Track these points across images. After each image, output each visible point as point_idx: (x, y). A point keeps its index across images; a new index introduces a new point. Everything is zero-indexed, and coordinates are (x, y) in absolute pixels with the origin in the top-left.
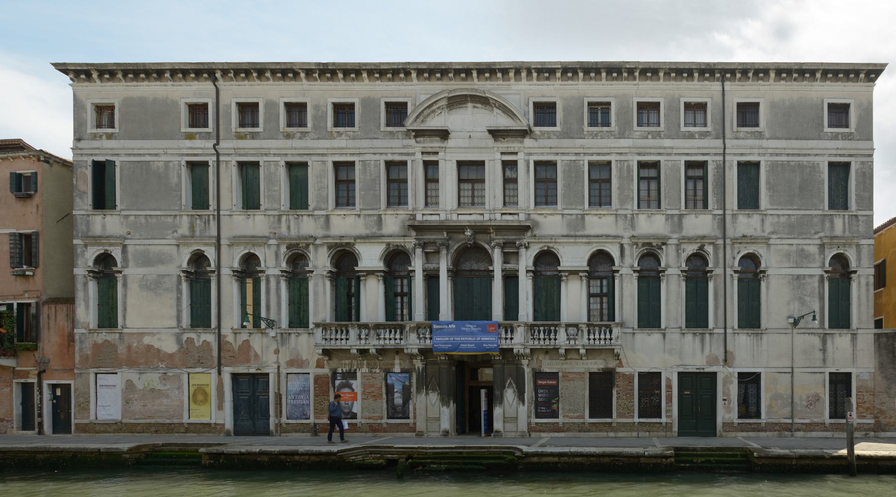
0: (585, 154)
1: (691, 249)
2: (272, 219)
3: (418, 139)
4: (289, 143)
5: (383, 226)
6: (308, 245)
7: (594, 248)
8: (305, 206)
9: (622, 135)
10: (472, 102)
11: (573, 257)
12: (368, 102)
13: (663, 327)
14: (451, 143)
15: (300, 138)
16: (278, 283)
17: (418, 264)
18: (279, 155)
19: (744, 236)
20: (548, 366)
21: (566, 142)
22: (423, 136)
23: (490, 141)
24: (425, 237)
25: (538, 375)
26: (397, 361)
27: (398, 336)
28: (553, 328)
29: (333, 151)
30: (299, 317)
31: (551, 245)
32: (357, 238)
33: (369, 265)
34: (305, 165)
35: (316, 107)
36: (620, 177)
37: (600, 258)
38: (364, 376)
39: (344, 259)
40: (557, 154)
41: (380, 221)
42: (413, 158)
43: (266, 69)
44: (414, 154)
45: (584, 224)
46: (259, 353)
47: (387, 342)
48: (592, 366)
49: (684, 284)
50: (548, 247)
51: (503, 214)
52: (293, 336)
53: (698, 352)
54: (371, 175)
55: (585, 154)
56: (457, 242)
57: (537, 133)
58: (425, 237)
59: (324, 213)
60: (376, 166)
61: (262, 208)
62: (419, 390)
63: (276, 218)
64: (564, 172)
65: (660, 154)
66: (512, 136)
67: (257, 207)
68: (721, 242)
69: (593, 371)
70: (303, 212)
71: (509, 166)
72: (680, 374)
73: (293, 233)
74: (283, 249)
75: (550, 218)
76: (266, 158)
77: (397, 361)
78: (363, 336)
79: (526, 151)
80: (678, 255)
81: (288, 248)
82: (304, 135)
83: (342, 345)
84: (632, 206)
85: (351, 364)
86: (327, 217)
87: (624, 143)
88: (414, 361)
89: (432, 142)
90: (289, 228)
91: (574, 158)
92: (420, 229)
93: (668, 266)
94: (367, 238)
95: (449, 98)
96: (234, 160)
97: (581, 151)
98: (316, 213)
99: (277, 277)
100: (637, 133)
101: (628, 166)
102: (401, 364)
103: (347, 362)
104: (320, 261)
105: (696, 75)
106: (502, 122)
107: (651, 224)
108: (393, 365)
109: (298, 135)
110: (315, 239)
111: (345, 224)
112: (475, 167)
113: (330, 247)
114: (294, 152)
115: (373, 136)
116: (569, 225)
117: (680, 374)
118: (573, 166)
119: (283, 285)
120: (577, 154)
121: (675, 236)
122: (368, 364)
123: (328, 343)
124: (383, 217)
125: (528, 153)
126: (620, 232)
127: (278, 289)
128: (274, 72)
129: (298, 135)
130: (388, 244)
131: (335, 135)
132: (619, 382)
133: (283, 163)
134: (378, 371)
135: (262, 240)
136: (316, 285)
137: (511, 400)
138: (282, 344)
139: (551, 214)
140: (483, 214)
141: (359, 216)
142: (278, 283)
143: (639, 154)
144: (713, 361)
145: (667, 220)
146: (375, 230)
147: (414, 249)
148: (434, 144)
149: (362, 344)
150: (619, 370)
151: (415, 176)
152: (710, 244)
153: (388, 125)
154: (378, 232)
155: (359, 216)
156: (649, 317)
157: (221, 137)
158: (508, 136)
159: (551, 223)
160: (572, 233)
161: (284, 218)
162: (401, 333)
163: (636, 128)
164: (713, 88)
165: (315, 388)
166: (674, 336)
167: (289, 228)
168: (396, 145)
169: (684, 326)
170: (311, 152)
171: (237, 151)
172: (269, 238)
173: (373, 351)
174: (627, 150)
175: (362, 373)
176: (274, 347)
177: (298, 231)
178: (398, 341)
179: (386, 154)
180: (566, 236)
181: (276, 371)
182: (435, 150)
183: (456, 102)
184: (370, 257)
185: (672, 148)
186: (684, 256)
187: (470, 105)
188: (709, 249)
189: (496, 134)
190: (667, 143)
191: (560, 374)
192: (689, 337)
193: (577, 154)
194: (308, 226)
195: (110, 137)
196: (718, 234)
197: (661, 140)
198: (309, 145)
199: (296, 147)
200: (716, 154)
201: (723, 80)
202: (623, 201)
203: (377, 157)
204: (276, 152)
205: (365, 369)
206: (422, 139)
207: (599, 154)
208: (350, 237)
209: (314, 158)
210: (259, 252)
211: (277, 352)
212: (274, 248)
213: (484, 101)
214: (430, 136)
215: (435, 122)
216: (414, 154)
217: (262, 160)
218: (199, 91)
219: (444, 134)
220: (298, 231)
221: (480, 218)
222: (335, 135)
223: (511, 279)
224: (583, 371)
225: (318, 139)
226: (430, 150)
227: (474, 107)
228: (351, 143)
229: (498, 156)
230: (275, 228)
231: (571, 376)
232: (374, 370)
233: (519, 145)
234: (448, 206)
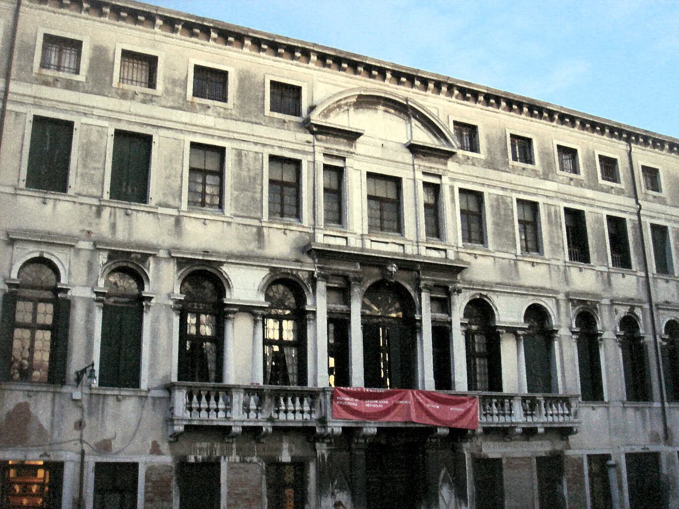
0: (512, 190)
1: (623, 311)
2: (86, 209)
3: (319, 136)
4: (126, 105)
5: (266, 243)
6: (146, 257)
7: (530, 301)
8: (143, 197)
9: (546, 177)
10: (384, 105)
11: (509, 312)
12: (245, 78)
13: (606, 400)
14: (360, 146)
15: (144, 102)
16: (89, 311)
17: (320, 304)
18: (109, 119)
19: (667, 302)
20: (492, 450)
21: (492, 174)
22: (327, 134)
23: (408, 157)
24: (335, 267)
25: (481, 462)
26: (285, 446)
27: (306, 408)
28: (507, 400)
29: (195, 129)
30: (121, 366)
31: (484, 293)
32: (230, 255)
33: (242, 298)
34: (147, 140)
35: (541, 144)
36: (550, 222)
37: (536, 313)
38: (231, 466)
39: (204, 281)
40: (483, 184)
41: (260, 235)
42: (310, 158)
43: (650, 137)
44: (313, 156)
45: (517, 271)
46: (46, 425)
47: (291, 416)
48: (540, 449)
49: (620, 351)
50: (481, 294)
51: (427, 248)
52: (111, 402)
53: (641, 430)
54: (249, 170)
55: (512, 190)
56: (370, 278)
57: (460, 156)
58: (335, 267)
59: (174, 212)
60: (256, 159)
61: (70, 192)
62: (321, 489)
63: (94, 209)
64: (492, 206)
65: (584, 204)
66: (435, 156)
67: (60, 185)
68: (647, 306)
69: (540, 454)
70: (142, 207)
71: (434, 189)
72: (628, 456)
73: (121, 235)
74: (103, 258)
75: (480, 259)
76: (85, 120)
77: (285, 446)
78: (253, 406)
79: (450, 175)
80: (612, 317)
81: (110, 258)
82: (148, 100)
83: (218, 419)
84: (564, 257)
85: (212, 449)
86: (178, 221)
87: (550, 185)
88: (317, 445)
89: (338, 143)
90: (113, 226)
91: (501, 193)
92: (324, 255)
93: (604, 330)
94: (244, 259)
95: (360, 96)
96: (32, 112)
97: (508, 186)
98: (161, 210)
99: (89, 301)
100: (561, 178)
101: (556, 212)
102: (290, 450)
103: (205, 445)
104: (164, 283)
105: (667, 147)
106: (423, 137)
107: (584, 280)
108: (280, 450)
109: (141, 97)
110: (157, 249)
111: (205, 234)
112: (383, 182)
113: (181, 263)
114: (133, 119)
115: (254, 120)
116: (502, 271)
117: (628, 456)
118: (500, 202)
119: (98, 316)
120: (503, 189)
121: (606, 295)
122: (239, 450)
123: (195, 416)
124: (265, 230)
125: (457, 175)
126: (555, 286)
127: (89, 320)
128: (323, 58)
129: (141, 97)
130: (273, 270)
131: (198, 107)
132: (567, 467)
133: (111, 132)
134: (255, 459)
135: (67, 243)
136: (156, 320)
137: (446, 499)
138: (90, 414)
139: (483, 256)
140: (403, 245)
141: (229, 223)
142: (89, 311)
143: (565, 200)
144: (655, 438)
145: (597, 276)
146: (253, 247)
147: (313, 281)
148: (340, 146)
149: (252, 419)
150: (568, 453)
151: (313, 183)
152: (639, 306)
153: (272, 110)
154: (259, 252)
155: (229, 223)
156: (592, 388)
157: (13, 77)
158: (431, 155)
159: (483, 267)
160: (506, 281)
161: (106, 213)
162: (312, 405)
163: (559, 172)
164: (620, 146)
165: (146, 487)
166: (616, 410)
167: (113, 226)
168: (288, 139)
169: (625, 399)
170: (160, 123)
171: (37, 102)
172: (77, 239)
173: (237, 430)
174: (553, 194)
175: (229, 463)
176: (74, 415)
177: (130, 234)
178: (306, 416)
179: (272, 146)
180: (499, 284)
181: (77, 458)
182: (341, 154)
183: (366, 101)
184: (245, 285)
185: (593, 200)
186: (617, 318)
187: (381, 108)
188: (638, 312)
189: (415, 149)
190: (589, 193)
191: (504, 462)
192: (630, 412)
193: (503, 189)
194: (143, 227)
195: (70, 86)
196: (644, 296)
197: (582, 189)
198: (157, 115)
199: (135, 114)
200: (631, 213)
201: (628, 140)
202: (553, 251)
203: (258, 149)
204: (103, 113)
205: (235, 458)
206: (324, 137)
207: (525, 193)
208: (217, 253)
209: (162, 132)
210: (59, 257)
211: (80, 425)
212: (84, 256)
213: (403, 109)
214: (335, 136)
215: (338, 120)
216: (313, 156)
217: (79, 122)
218: (615, 149)
219: (352, 136)
220: (130, 234)
221: (342, 242)
222: (198, 107)
223: (442, 335)
224: (529, 455)
225: (173, 108)
226: (335, 153)
227: (386, 111)
228: (222, 123)
229: (421, 178)
230: (90, 224)
231: (517, 462)
232: (248, 459)
233: (347, 149)
234: (357, 231)
